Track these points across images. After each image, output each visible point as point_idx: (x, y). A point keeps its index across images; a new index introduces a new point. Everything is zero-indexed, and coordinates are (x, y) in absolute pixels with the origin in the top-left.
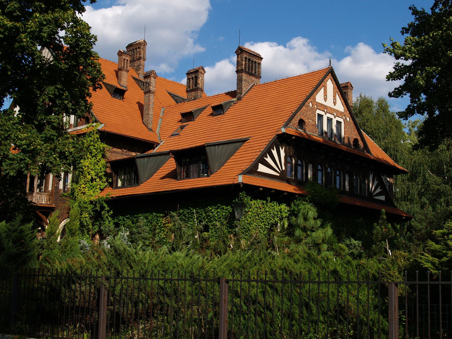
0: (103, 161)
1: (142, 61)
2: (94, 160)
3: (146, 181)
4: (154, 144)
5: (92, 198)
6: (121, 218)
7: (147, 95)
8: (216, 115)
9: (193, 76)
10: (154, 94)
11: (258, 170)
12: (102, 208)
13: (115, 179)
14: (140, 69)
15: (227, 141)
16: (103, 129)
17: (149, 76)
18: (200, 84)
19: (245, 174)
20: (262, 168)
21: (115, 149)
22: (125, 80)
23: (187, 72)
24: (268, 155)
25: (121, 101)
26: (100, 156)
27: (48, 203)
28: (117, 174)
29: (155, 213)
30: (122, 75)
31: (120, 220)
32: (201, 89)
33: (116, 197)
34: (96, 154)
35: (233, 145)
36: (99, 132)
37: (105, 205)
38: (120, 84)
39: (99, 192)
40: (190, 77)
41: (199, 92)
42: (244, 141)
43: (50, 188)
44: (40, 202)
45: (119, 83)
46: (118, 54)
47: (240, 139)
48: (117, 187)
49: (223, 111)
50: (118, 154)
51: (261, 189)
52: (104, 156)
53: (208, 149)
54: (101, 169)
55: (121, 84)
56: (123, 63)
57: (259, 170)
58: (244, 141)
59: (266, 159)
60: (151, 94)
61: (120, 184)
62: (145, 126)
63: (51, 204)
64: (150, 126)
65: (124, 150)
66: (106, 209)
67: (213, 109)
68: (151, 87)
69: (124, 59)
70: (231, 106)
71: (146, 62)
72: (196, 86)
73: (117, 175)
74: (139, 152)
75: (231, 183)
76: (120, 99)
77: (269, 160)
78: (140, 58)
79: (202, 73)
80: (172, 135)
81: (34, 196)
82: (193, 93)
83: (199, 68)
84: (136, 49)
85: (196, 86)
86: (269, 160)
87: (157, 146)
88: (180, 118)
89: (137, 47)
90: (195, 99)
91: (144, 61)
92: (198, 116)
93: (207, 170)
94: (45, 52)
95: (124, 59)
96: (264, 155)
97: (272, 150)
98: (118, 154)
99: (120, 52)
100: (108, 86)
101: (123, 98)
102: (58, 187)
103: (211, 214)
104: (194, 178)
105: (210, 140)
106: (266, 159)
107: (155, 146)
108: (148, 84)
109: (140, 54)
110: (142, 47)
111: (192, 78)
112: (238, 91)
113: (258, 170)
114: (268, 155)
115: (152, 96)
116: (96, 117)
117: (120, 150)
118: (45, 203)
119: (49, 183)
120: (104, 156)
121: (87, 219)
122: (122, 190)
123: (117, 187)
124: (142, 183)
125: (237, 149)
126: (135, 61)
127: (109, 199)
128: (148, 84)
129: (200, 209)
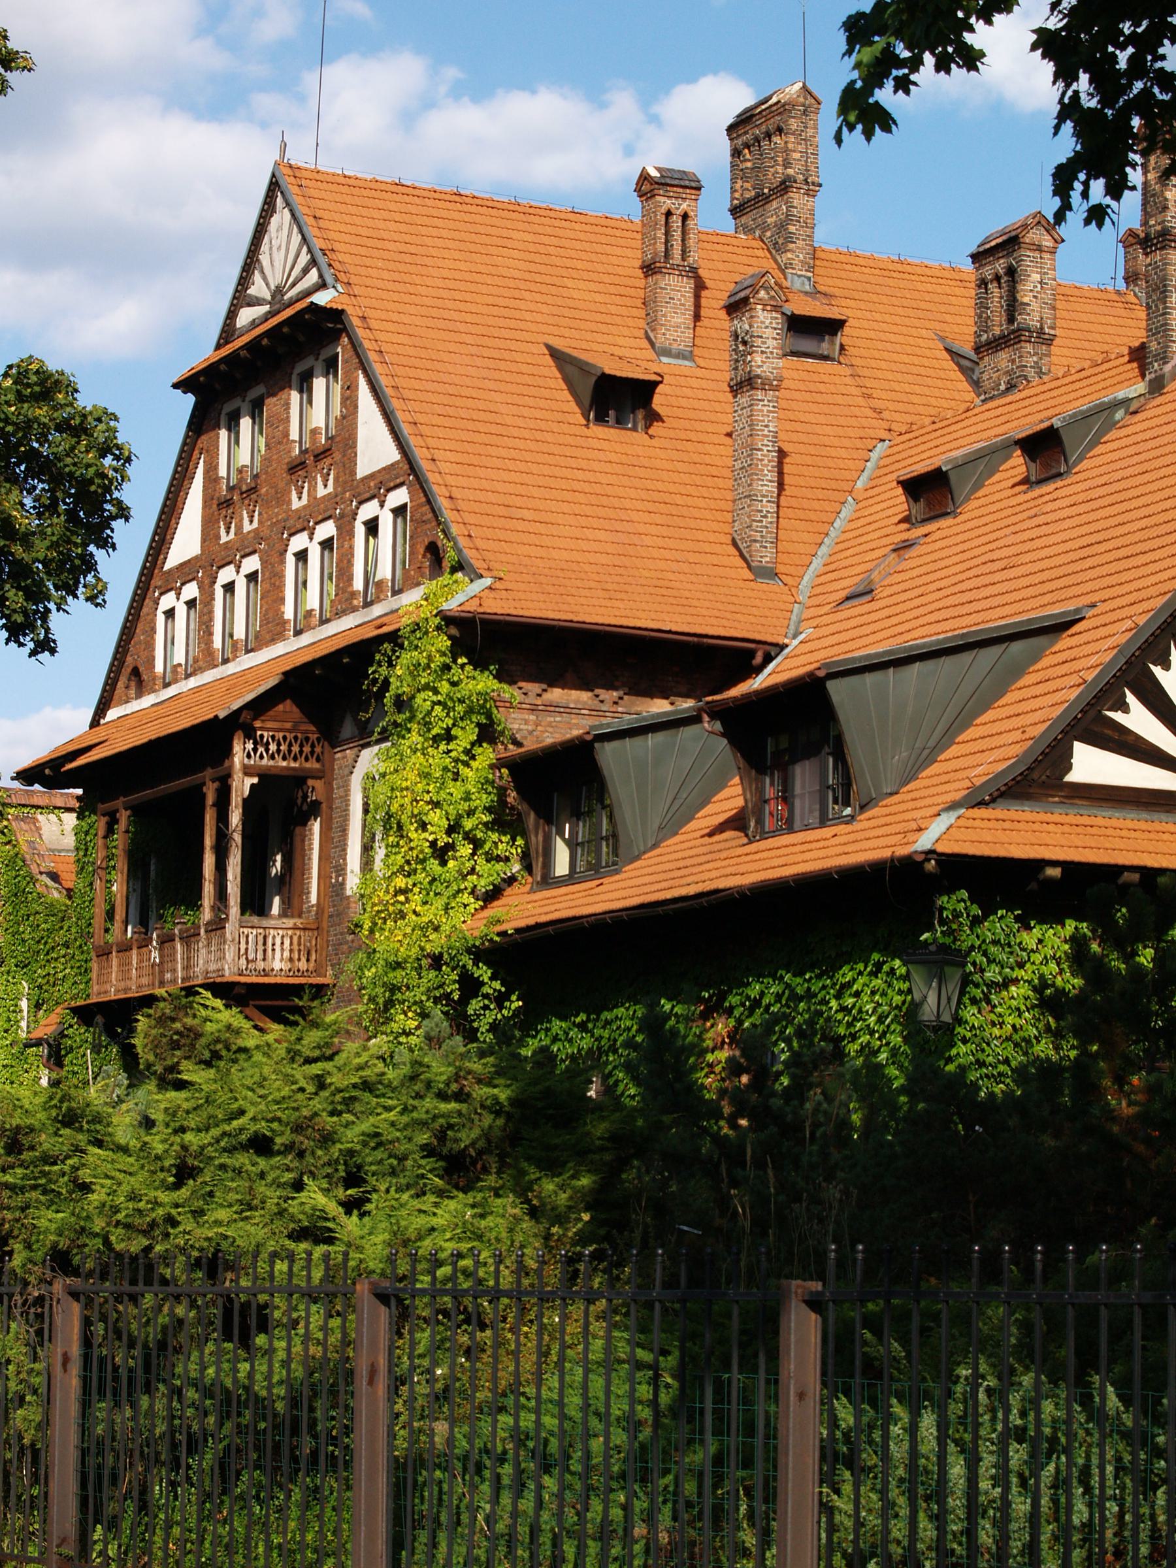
0: (486, 755)
1: (797, 198)
2: (437, 759)
3: (655, 846)
4: (751, 654)
5: (436, 943)
6: (557, 1025)
7: (744, 400)
8: (1040, 482)
9: (1000, 266)
10: (777, 389)
11: (1071, 777)
12: (470, 986)
13: (537, 840)
14: (789, 239)
15: (938, 642)
16: (472, 606)
17: (745, 301)
18: (1035, 306)
19: (981, 804)
20: (1091, 765)
21: (556, 694)
22: (678, 319)
23: (973, 248)
24: (1131, 698)
25: (640, 437)
26: (466, 735)
27: (303, 965)
28: (549, 817)
29: (669, 999)
30: (661, 295)
31: (555, 1039)
32: (1041, 332)
33: (518, 931)
34: (448, 730)
35: (994, 651)
36: (449, 620)
37: (483, 972)
38: (652, 344)
39: (471, 909)
40: (988, 272)
41: (1029, 348)
42: (1060, 627)
43: (314, 899)
44: (261, 965)
45: (648, 338)
46: (638, 190)
47: (877, 655)
48: (548, 880)
49: (1066, 461)
50: (549, 715)
51: (1054, 872)
52: (488, 734)
53: (835, 688)
54: (467, 797)
55: (660, 341)
56: (660, 233)
57: (1073, 777)
58: (1060, 627)
59: (1118, 716)
60: (759, 395)
61: (562, 867)
62: (742, 555)
63: (317, 972)
64: (765, 556)
65: (604, 694)
66: (486, 990)
67: (904, 488)
68: (758, 359)
69: (669, 214)
70: (1112, 425)
71: (821, 202)
72: (1011, 320)
73: (549, 822)
74: (687, 696)
75: (886, 854)
76: (634, 429)
77: (1138, 719)
78: (784, 187)
79: (1039, 248)
80: (848, 598)
81: (228, 936)
82: (1003, 358)
83: (1025, 226)
84: (768, 135)
85: (1011, 320)
86: (1138, 719)
87: (768, 659)
88: (899, 502)
89: (771, 125)
90: (1011, 387)
91: (811, 194)
92: (978, 486)
93: (846, 793)
94: (280, 229)
95: (669, 214)
96: (1107, 694)
97: (1157, 671)
98: (549, 715)
99: (644, 177)
100: (569, 369)
101: (653, 417)
102: (343, 884)
103: (851, 1001)
104: (807, 828)
105: (845, 647)
106: (1118, 716)
107: (758, 659)
108: (745, 343)
109: (787, 164)
110: (793, 124)
111: (997, 278)
112: (1154, 346)
113: (1071, 777)
114: (1131, 698)
115: (764, 404)
116: (462, 542)
117: (584, 696)
118: (286, 966)
119: (310, 869)
120: (488, 734)
121: (413, 1040)
122: (570, 891)
123: (548, 880)
124: (637, 858)
125: (1017, 671)
126: (767, 200)
127: (491, 940)
128: (745, 343)
129: (819, 977)
